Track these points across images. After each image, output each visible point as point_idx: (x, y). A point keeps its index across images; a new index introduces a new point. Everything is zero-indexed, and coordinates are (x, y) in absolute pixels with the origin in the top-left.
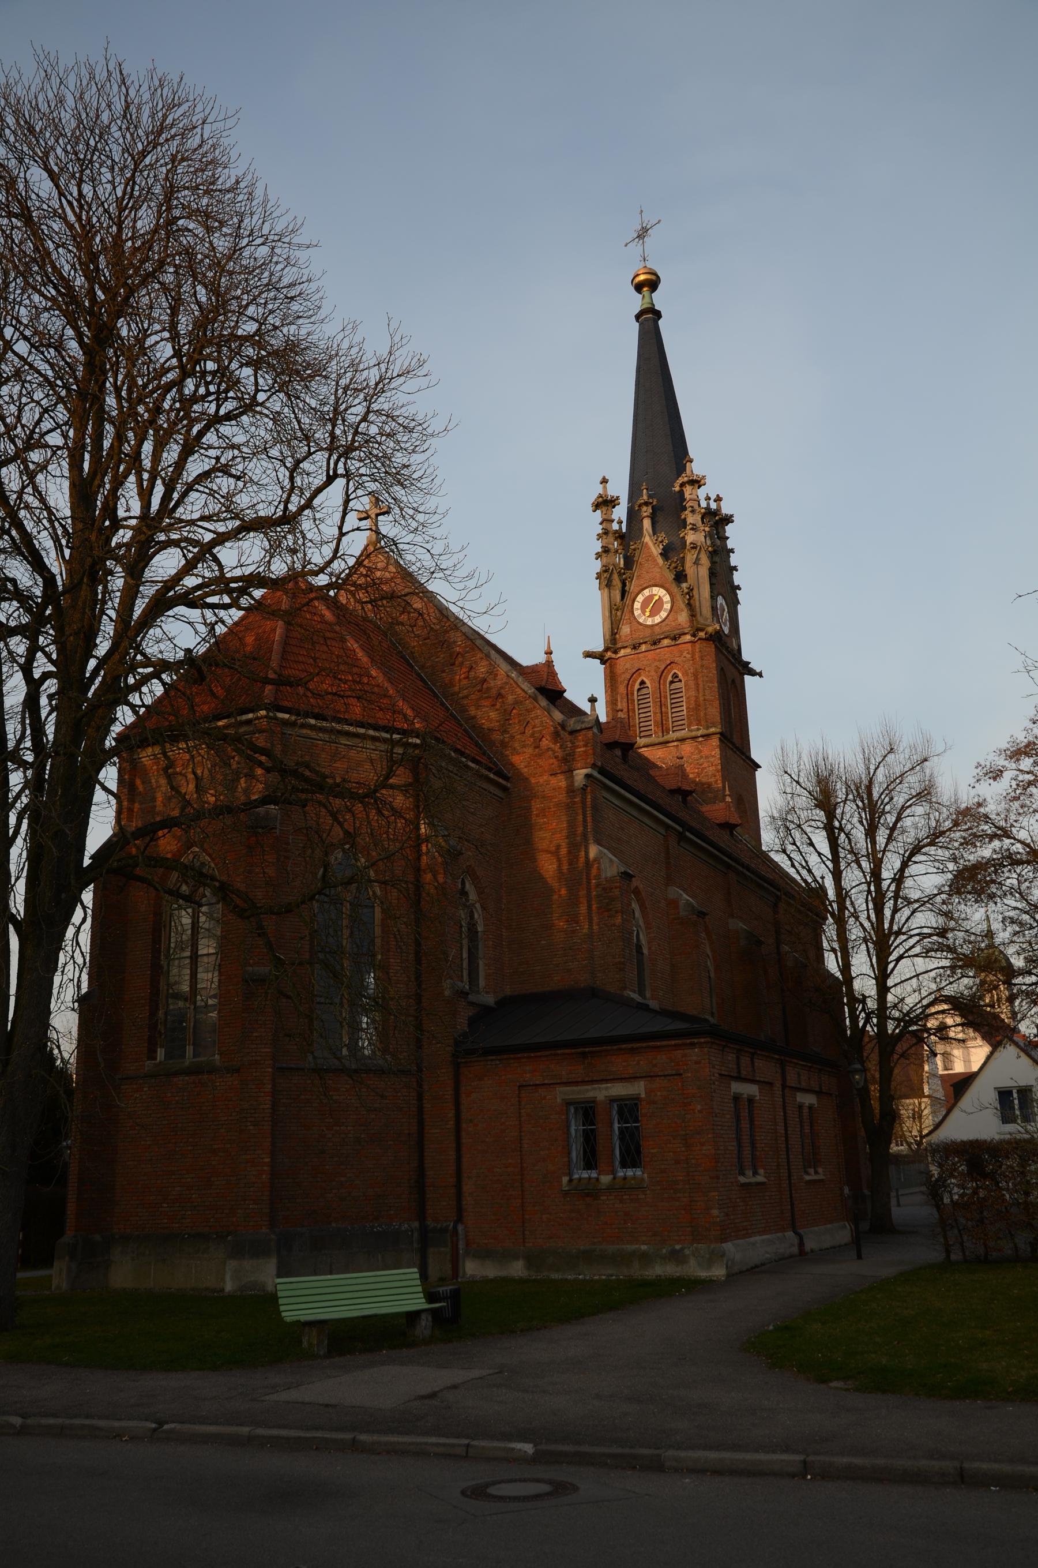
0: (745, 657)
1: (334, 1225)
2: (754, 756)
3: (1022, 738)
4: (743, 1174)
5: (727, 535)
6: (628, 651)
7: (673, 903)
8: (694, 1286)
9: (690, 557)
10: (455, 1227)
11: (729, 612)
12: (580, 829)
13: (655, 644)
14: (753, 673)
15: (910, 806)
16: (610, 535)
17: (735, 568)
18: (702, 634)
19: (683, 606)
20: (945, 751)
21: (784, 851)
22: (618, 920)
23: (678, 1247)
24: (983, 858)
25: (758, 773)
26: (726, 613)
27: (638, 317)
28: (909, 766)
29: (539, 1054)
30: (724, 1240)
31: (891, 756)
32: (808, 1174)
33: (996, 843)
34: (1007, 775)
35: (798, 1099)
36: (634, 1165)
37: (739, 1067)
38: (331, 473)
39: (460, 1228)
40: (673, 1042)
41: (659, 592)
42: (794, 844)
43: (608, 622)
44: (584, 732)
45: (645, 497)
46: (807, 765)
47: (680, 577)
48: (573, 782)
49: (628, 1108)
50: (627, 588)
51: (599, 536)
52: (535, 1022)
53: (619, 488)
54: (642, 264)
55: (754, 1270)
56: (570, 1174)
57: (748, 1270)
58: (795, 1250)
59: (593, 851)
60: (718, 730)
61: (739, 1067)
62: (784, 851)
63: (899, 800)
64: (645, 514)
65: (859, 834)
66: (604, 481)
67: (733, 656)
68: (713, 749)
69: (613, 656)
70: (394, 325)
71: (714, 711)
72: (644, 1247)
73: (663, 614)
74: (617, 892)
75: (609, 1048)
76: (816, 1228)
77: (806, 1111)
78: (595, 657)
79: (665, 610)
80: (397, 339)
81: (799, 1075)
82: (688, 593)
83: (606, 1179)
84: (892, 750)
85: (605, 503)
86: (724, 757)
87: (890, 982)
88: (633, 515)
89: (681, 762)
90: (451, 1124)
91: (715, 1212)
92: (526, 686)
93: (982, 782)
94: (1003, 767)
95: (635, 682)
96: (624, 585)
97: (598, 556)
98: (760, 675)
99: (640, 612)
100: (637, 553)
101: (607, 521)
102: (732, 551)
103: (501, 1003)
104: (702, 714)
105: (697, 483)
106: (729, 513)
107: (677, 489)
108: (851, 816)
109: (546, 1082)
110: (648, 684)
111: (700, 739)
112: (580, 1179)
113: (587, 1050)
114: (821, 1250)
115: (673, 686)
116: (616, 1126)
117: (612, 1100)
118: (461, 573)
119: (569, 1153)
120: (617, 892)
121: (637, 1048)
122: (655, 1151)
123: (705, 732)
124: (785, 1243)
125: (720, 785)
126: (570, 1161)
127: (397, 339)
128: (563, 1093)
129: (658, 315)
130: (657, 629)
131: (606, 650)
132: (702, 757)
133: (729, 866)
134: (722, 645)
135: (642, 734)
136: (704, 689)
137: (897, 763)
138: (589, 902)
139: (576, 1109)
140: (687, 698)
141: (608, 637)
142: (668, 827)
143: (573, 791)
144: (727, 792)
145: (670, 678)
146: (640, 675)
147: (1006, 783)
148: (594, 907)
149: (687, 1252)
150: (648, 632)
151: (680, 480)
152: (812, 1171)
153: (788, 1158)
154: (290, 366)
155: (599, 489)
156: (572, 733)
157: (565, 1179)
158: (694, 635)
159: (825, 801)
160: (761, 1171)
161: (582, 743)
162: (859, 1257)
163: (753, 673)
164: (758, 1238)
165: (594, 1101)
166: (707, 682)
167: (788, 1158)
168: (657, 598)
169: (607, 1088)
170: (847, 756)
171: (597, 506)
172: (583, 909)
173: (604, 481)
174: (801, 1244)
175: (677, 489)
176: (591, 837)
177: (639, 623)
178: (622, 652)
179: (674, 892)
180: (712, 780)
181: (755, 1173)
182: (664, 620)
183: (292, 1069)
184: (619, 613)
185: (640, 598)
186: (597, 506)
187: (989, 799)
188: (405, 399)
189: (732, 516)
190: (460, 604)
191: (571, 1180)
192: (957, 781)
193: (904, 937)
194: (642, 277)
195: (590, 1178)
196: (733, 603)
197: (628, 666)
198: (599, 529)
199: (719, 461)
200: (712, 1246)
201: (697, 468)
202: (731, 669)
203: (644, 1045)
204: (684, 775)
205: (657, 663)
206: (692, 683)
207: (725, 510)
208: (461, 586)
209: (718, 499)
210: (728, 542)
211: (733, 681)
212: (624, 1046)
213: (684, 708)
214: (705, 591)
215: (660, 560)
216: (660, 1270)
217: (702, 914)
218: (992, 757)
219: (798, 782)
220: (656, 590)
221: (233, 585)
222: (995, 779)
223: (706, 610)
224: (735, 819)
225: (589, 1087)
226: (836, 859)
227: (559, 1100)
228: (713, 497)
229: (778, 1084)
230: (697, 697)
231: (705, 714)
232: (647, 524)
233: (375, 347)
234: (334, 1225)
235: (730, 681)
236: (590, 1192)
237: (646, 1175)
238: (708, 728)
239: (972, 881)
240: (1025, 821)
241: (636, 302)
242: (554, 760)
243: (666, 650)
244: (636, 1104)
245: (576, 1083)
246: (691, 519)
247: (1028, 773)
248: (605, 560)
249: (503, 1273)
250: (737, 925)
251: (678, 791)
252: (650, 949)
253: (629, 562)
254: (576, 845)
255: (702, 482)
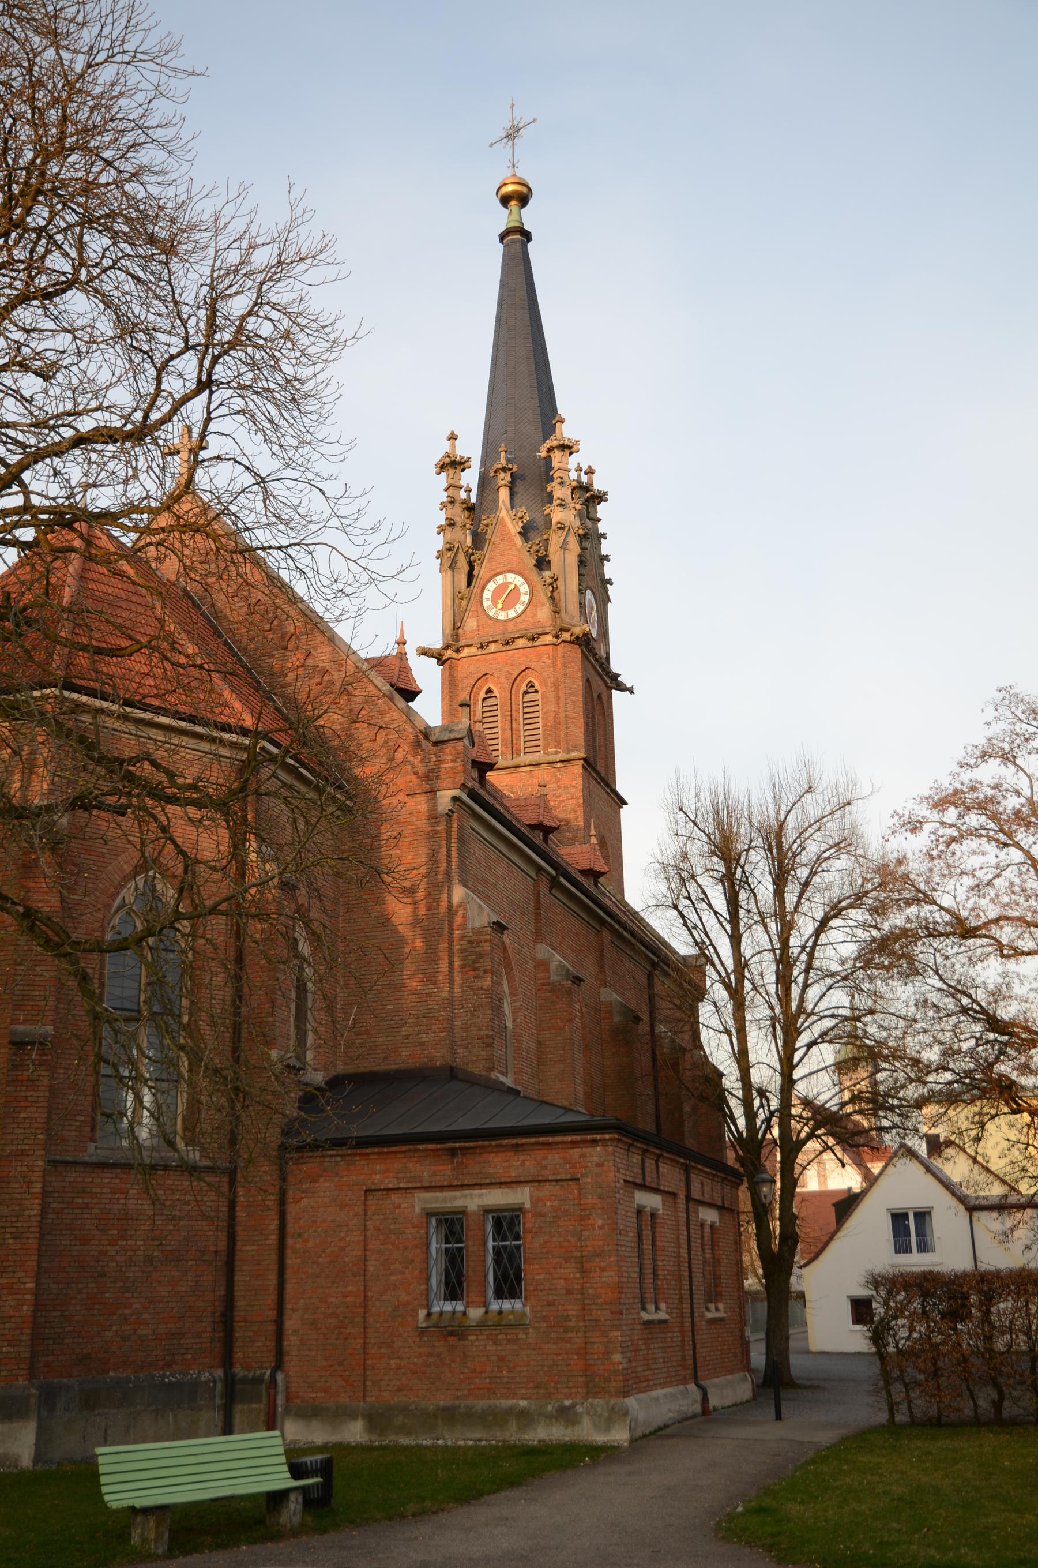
0: (615, 667)
1: (112, 1374)
2: (620, 788)
3: (948, 785)
4: (644, 1309)
5: (599, 516)
6: (473, 650)
7: (543, 965)
8: (600, 1455)
9: (556, 540)
10: (273, 1376)
11: (597, 611)
12: (443, 866)
13: (507, 643)
14: (621, 687)
15: (829, 858)
16: (457, 505)
17: (606, 558)
18: (566, 636)
19: (545, 600)
20: (871, 794)
21: (676, 907)
22: (487, 982)
23: (567, 1403)
24: (896, 927)
25: (624, 811)
26: (594, 613)
27: (502, 237)
28: (828, 810)
29: (394, 1149)
30: (626, 1394)
31: (808, 796)
32: (708, 1309)
33: (913, 910)
34: (928, 827)
35: (701, 1216)
36: (513, 1294)
37: (643, 1174)
38: (204, 379)
39: (280, 1377)
40: (569, 1138)
41: (515, 580)
42: (689, 898)
43: (450, 612)
44: (452, 743)
45: (503, 462)
46: (706, 801)
47: (542, 563)
48: (435, 806)
49: (506, 1222)
50: (475, 573)
51: (443, 506)
52: (387, 1107)
53: (471, 448)
54: (510, 172)
55: (658, 1433)
56: (429, 1306)
57: (651, 1434)
58: (698, 1408)
59: (459, 893)
60: (583, 755)
61: (643, 1174)
62: (676, 907)
63: (813, 848)
64: (502, 482)
65: (765, 889)
66: (453, 437)
67: (601, 665)
68: (574, 777)
69: (455, 655)
70: (296, 193)
71: (577, 732)
72: (523, 1403)
73: (520, 608)
74: (487, 947)
75: (486, 1143)
76: (716, 1380)
77: (707, 1230)
78: (432, 656)
79: (523, 603)
80: (299, 212)
81: (702, 1183)
82: (551, 584)
83: (475, 1313)
84: (810, 790)
85: (453, 464)
86: (586, 788)
87: (797, 1074)
88: (485, 481)
89: (544, 791)
90: (273, 1239)
91: (617, 1357)
92: (379, 681)
93: (897, 835)
94: (924, 817)
95: (480, 689)
96: (472, 568)
97: (441, 529)
98: (632, 692)
99: (490, 602)
100: (490, 529)
101: (453, 486)
102: (604, 536)
103: (335, 1083)
104: (562, 734)
105: (567, 448)
106: (603, 489)
107: (544, 454)
108: (759, 870)
109: (402, 1185)
110: (496, 693)
111: (559, 765)
112: (441, 1313)
113: (457, 1145)
114: (723, 1408)
115: (528, 697)
116: (491, 1244)
117: (487, 1211)
118: (365, 523)
119: (428, 1279)
120: (487, 947)
121: (522, 1145)
122: (541, 1277)
123: (565, 756)
124: (688, 1399)
125: (581, 823)
126: (428, 1290)
127: (299, 212)
128: (423, 1201)
129: (527, 236)
130: (511, 626)
131: (447, 647)
132: (559, 787)
133: (603, 923)
134: (590, 651)
135: (527, 750)
136: (566, 703)
137: (814, 806)
138: (451, 956)
139: (439, 1222)
140: (544, 714)
141: (448, 631)
142: (539, 869)
143: (436, 818)
144: (593, 832)
145: (524, 688)
146: (486, 681)
147: (922, 840)
148: (457, 963)
149: (579, 1409)
150: (499, 629)
151: (548, 444)
152: (712, 1306)
153: (691, 1290)
154: (155, 238)
155: (446, 447)
156: (436, 743)
157: (422, 1313)
158: (557, 637)
159: (726, 850)
160: (663, 1306)
161: (449, 757)
162: (779, 1417)
163: (621, 687)
164: (659, 1392)
165: (463, 1212)
166: (571, 694)
167: (691, 1290)
168: (512, 587)
169: (480, 1196)
170: (753, 793)
171: (442, 467)
172: (443, 966)
173: (453, 437)
174: (705, 1400)
175: (544, 454)
176: (455, 876)
177: (488, 616)
178: (466, 652)
179: (543, 951)
180: (572, 816)
181: (657, 1308)
182: (519, 616)
183: (67, 1163)
184: (464, 603)
185: (491, 586)
186: (442, 467)
187: (909, 855)
188: (313, 292)
189: (606, 493)
190: (363, 562)
191: (429, 1315)
192: (878, 832)
193: (816, 1018)
194: (510, 188)
195: (454, 1312)
196: (603, 600)
197: (472, 669)
198: (444, 497)
199: (596, 423)
200: (612, 1402)
201: (567, 431)
202: (600, 682)
203: (533, 1140)
204: (547, 809)
205: (508, 668)
206: (551, 695)
207: (598, 486)
208: (359, 540)
209: (590, 472)
210: (600, 524)
211: (599, 696)
212: (506, 1141)
213: (540, 725)
214: (572, 582)
215: (519, 541)
216: (548, 1433)
217: (577, 980)
218: (910, 805)
219: (694, 823)
220: (511, 577)
221: (42, 516)
222: (913, 831)
223: (573, 607)
224: (600, 866)
225: (457, 1193)
226: (734, 918)
227: (417, 1210)
228: (585, 468)
229: (682, 1195)
230: (557, 713)
231: (567, 735)
232: (504, 494)
233: (270, 219)
234: (112, 1374)
235: (595, 696)
236: (454, 1330)
237: (528, 1309)
238: (569, 751)
239: (890, 953)
240: (950, 884)
241: (502, 219)
242: (413, 777)
243: (520, 655)
244: (518, 1217)
245: (441, 1188)
246: (560, 493)
247: (951, 826)
248: (449, 535)
249: (335, 1438)
250: (609, 995)
251: (539, 827)
252: (514, 1021)
253: (479, 541)
254: (437, 885)
255: (575, 448)
